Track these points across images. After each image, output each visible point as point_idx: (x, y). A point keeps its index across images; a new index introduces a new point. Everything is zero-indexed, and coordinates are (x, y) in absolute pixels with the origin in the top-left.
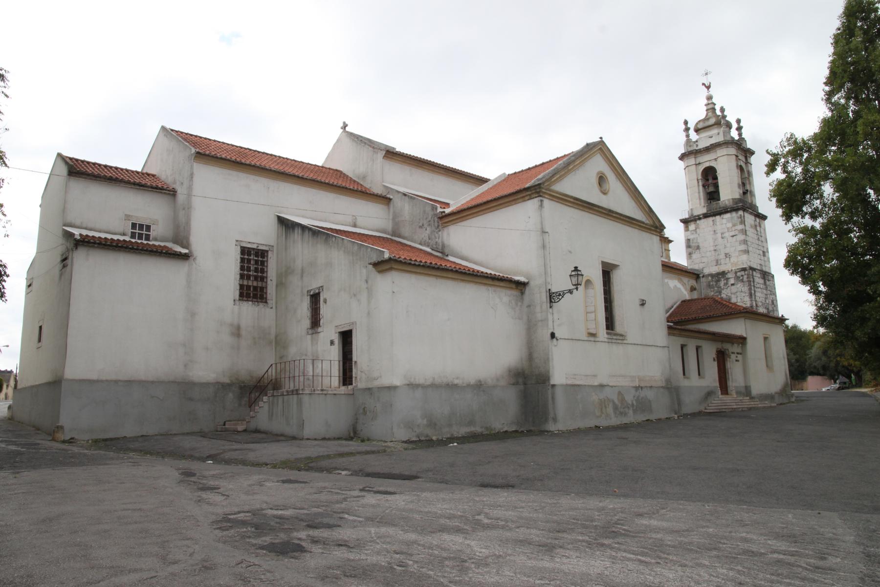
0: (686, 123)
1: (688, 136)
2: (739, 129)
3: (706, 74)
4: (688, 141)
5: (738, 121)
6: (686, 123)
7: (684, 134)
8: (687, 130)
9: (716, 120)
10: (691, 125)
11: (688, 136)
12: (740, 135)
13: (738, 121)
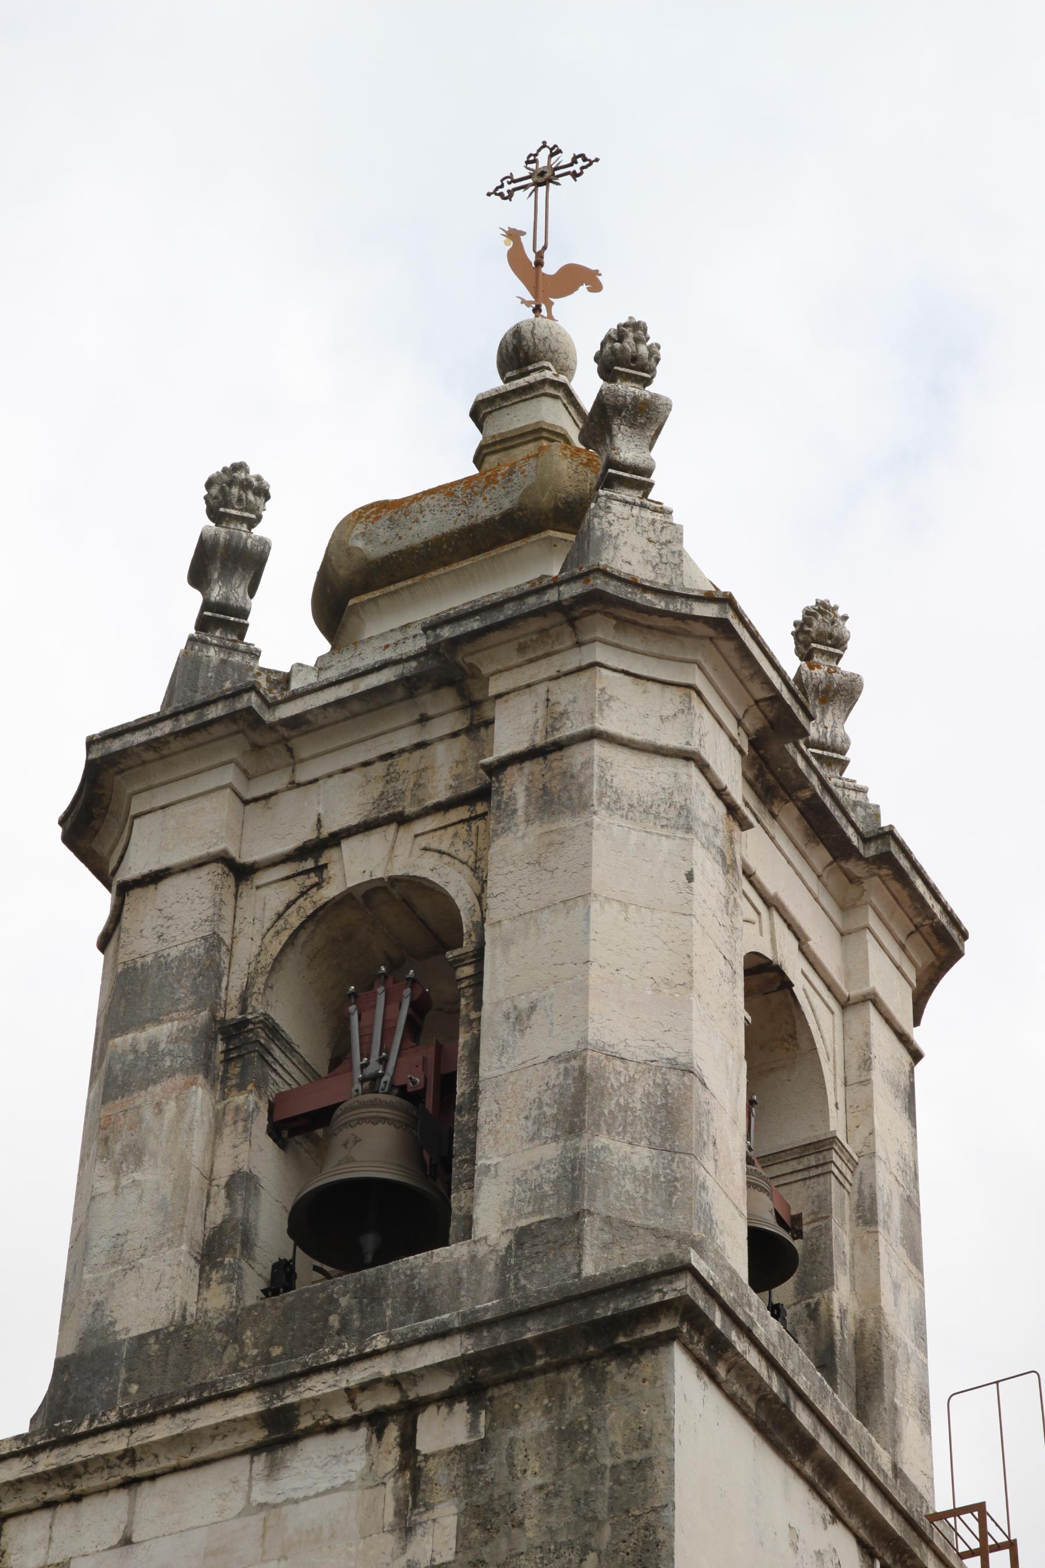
1: (221, 622)
3: (544, 178)
6: (234, 495)
9: (558, 463)
11: (221, 622)
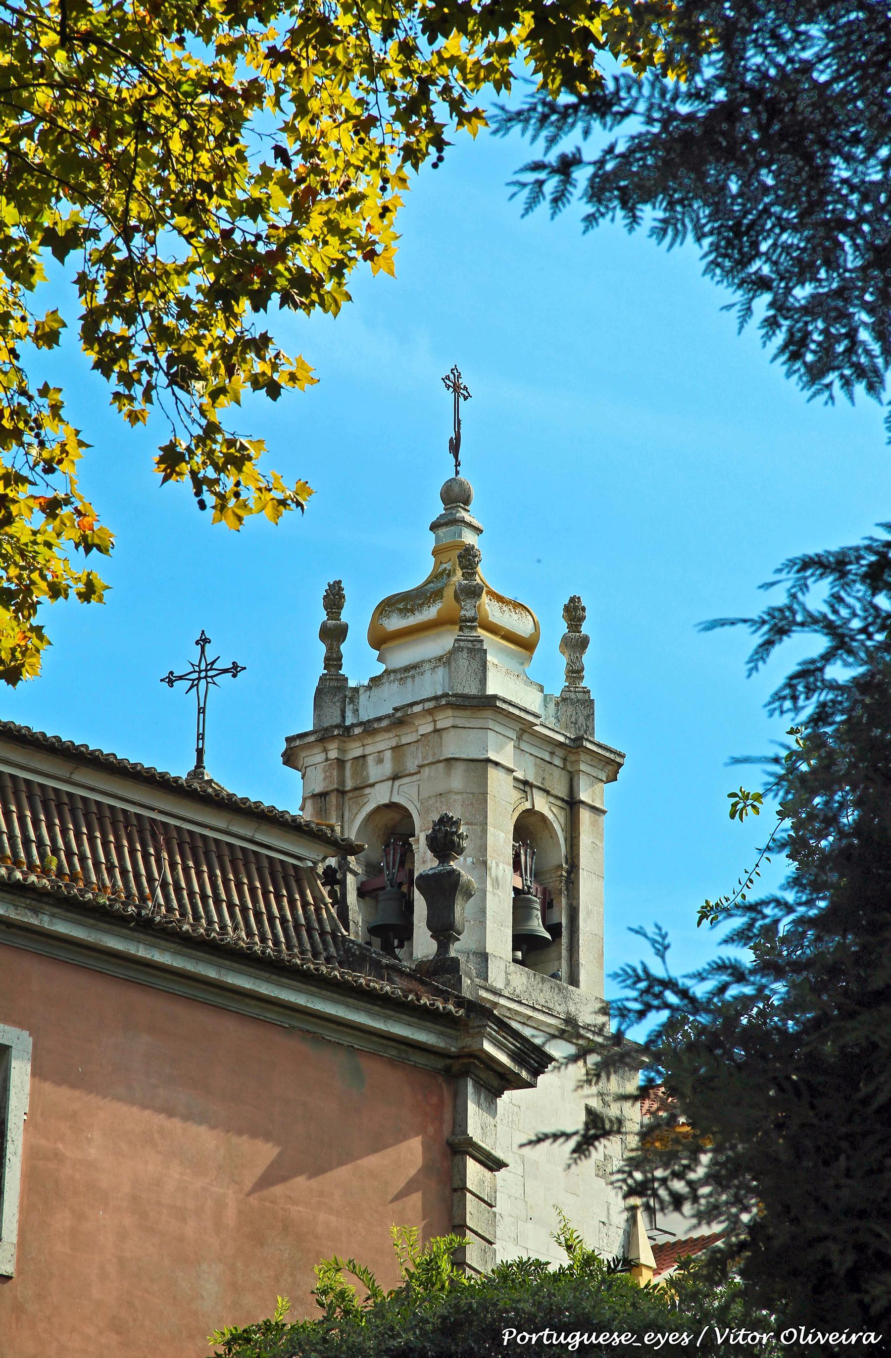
0: (334, 599)
1: (333, 661)
2: (576, 644)
4: (332, 688)
5: (574, 612)
6: (334, 599)
7: (321, 649)
8: (334, 634)
10: (357, 617)
11: (333, 661)
12: (575, 673)
13: (574, 612)
